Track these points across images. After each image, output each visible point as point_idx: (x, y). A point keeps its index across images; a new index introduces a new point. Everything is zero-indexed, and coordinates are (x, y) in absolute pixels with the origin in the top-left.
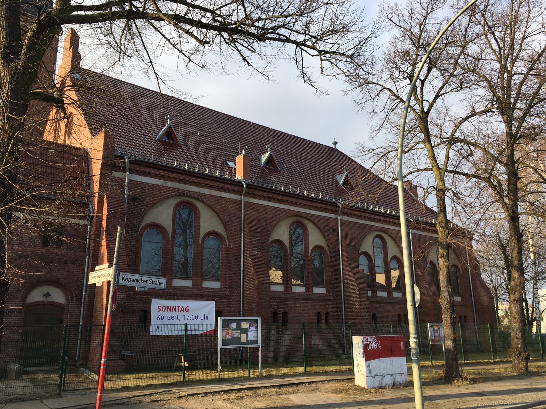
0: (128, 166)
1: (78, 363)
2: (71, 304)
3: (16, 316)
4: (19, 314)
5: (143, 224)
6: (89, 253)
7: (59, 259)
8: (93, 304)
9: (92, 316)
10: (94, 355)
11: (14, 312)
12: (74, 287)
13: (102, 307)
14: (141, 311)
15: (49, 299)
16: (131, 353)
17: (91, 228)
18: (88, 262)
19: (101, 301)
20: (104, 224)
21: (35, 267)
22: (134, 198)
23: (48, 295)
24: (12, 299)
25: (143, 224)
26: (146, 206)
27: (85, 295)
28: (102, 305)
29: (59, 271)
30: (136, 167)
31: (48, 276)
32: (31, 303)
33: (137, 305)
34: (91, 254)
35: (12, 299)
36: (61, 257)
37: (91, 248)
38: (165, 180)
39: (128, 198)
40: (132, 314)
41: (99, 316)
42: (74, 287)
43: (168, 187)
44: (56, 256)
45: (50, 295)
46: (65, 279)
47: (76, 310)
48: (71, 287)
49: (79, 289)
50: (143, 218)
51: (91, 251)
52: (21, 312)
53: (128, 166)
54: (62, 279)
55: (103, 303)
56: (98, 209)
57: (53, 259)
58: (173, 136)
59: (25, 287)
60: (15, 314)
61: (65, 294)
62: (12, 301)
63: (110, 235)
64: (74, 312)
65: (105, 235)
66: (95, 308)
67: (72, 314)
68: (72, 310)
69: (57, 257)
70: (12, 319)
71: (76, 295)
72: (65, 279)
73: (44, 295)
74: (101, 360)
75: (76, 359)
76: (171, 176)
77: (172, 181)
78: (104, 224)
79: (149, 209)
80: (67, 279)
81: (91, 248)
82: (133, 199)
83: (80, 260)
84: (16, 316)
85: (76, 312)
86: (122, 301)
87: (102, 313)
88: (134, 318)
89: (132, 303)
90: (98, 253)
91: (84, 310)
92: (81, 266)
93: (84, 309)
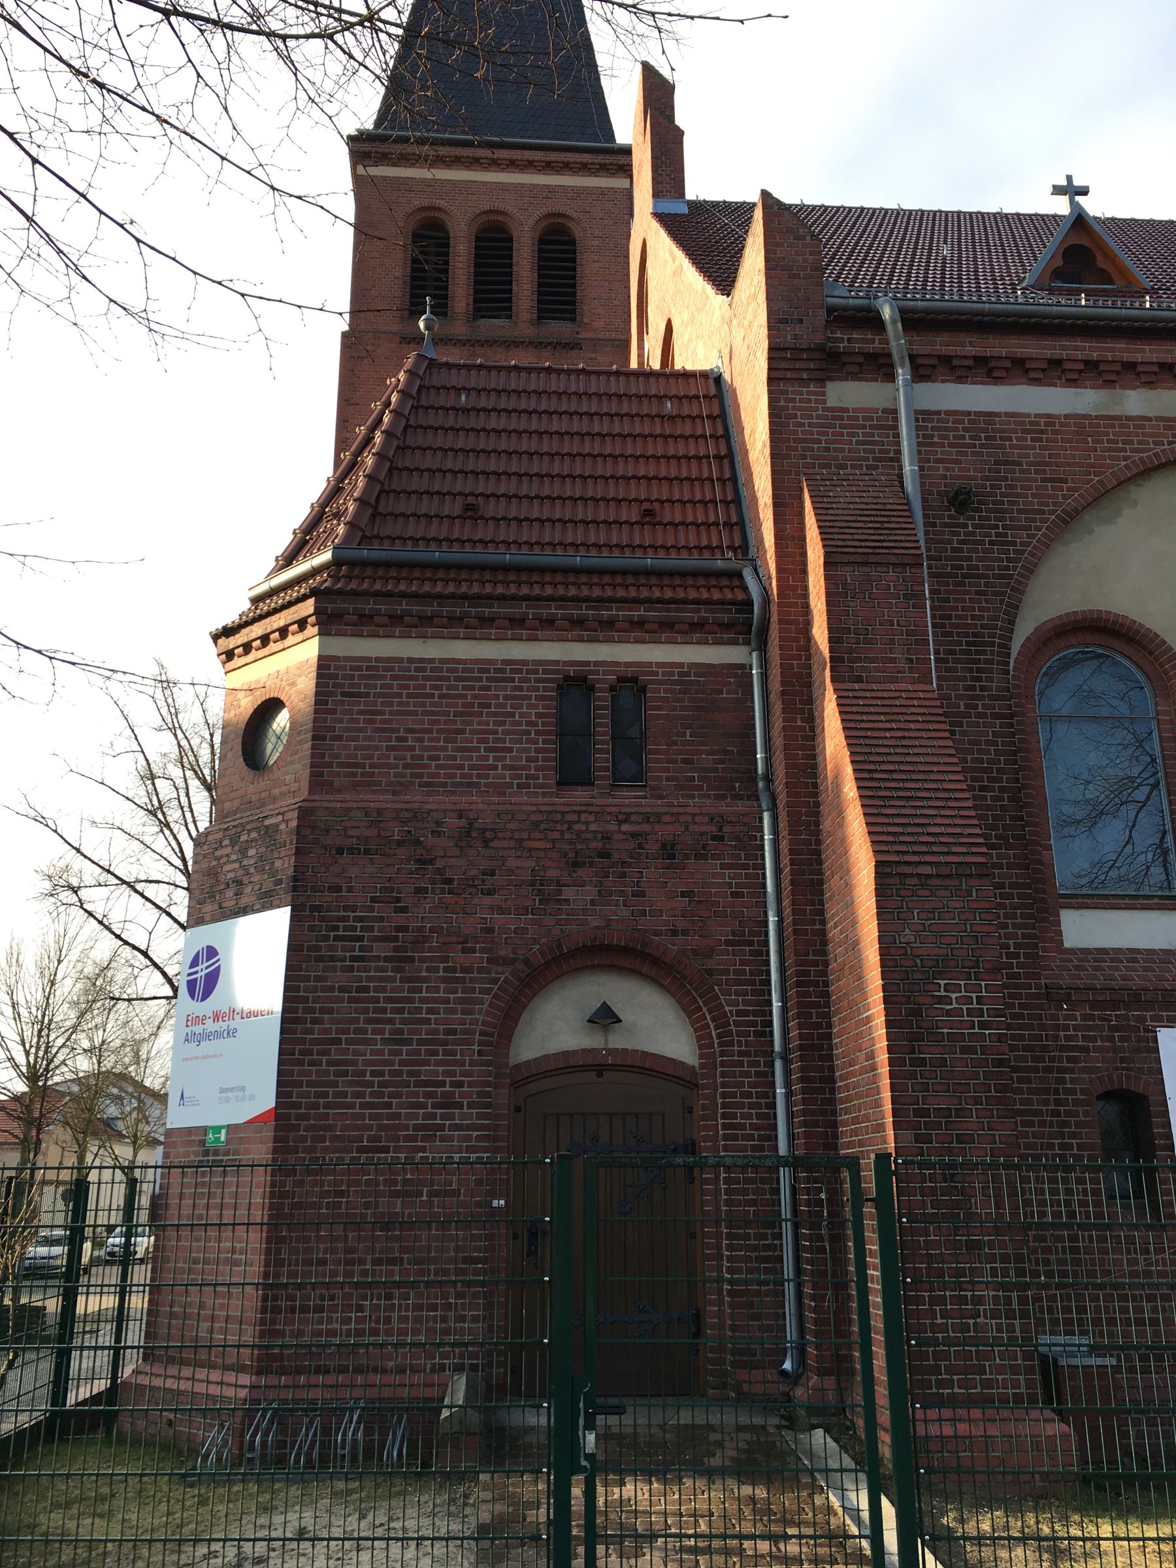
0: (896, 340)
1: (799, 1392)
2: (723, 1064)
3: (469, 1128)
4: (480, 1116)
5: (1024, 630)
6: (773, 799)
7: (634, 835)
8: (830, 1058)
9: (834, 1125)
10: (417, 1238)
11: (460, 1106)
12: (727, 972)
13: (873, 1068)
14: (1105, 1096)
15: (618, 1041)
16: (1095, 1350)
17: (764, 676)
18: (776, 843)
19: (860, 1035)
20: (820, 633)
21: (533, 883)
22: (955, 497)
23: (605, 1018)
24: (445, 1042)
25: (1024, 630)
26: (1029, 528)
27: (784, 1010)
28: (871, 1056)
29: (642, 894)
30: (941, 344)
31: (594, 922)
32: (537, 1060)
33: (1071, 1059)
34: (782, 799)
35: (445, 1042)
36: (646, 828)
37: (780, 772)
38: (1109, 384)
39: (924, 500)
40: (1056, 1113)
41: (867, 1118)
42: (727, 972)
43: (1129, 418)
44: (620, 823)
45: (620, 1021)
46: (674, 933)
47: (750, 1094)
48: (710, 972)
49: (753, 983)
50: (1019, 590)
51: (780, 787)
52: (487, 1105)
53: (896, 340)
54: (658, 933)
55: (872, 1042)
56: (779, 570)
57: (606, 838)
58: (1101, 263)
59: (496, 981)
60: (465, 1117)
61: (689, 1010)
62: (445, 1053)
63: (859, 680)
64: (742, 1105)
65: (832, 681)
66: (842, 1078)
67: (734, 1116)
68: (734, 1095)
69: (625, 828)
70: (451, 1138)
71: (740, 1013)
72: (674, 933)
73: (590, 1021)
74: (155, 1289)
75: (787, 1365)
76: (1139, 358)
77: (1149, 385)
78: (820, 633)
79: (1047, 545)
80: (685, 932)
81: (780, 772)
82: (952, 502)
83: (737, 838)
84: (469, 1128)
85: (751, 1106)
86: (982, 1026)
87: (878, 1104)
88: (1073, 1135)
89: (1045, 1048)
90: (815, 785)
91: (789, 1094)
92: (746, 867)
93: (788, 1084)
